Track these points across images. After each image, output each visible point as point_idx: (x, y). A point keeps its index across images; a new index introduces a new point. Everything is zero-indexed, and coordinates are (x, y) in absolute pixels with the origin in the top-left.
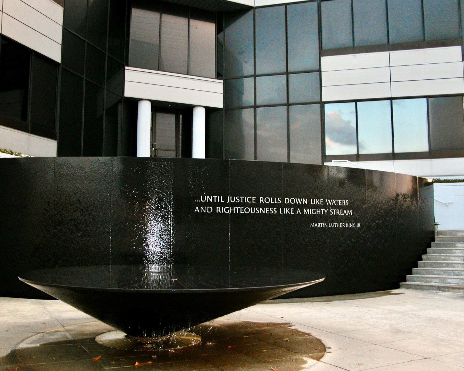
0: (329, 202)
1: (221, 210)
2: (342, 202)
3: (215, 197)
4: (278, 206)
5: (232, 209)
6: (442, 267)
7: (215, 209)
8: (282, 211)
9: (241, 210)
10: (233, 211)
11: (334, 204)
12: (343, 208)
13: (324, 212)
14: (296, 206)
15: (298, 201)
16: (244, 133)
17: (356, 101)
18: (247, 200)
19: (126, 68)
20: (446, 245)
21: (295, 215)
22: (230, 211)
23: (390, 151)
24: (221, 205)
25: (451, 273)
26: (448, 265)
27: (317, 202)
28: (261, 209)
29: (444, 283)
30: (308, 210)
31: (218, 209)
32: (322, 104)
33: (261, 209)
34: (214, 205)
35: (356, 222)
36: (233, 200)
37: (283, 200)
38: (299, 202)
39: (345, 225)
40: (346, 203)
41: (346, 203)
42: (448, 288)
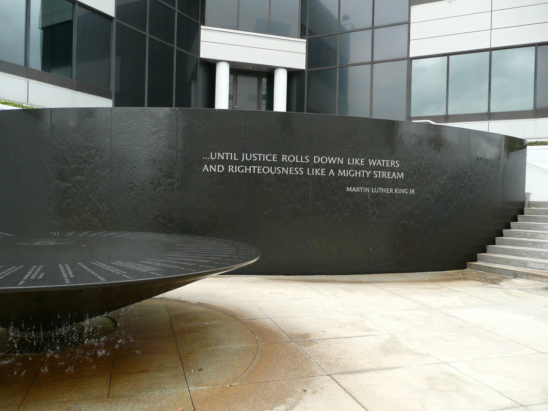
0: (372, 162)
1: (234, 169)
2: (390, 162)
3: (227, 154)
4: (305, 166)
5: (248, 168)
6: (526, 246)
7: (226, 168)
8: (311, 172)
9: (259, 170)
10: (358, 175)
11: (379, 165)
12: (392, 170)
13: (365, 174)
14: (328, 167)
15: (331, 160)
16: (349, 101)
17: (448, 55)
18: (266, 157)
19: (202, 27)
20: (537, 220)
21: (328, 178)
22: (244, 171)
23: (485, 110)
24: (234, 163)
25: (536, 255)
26: (534, 244)
27: (356, 161)
28: (283, 168)
29: (524, 267)
30: (344, 171)
31: (231, 169)
32: (410, 60)
33: (283, 168)
34: (226, 163)
35: (410, 187)
36: (249, 158)
37: (311, 159)
38: (332, 161)
39: (394, 191)
40: (395, 164)
41: (395, 164)
42: (535, 275)
